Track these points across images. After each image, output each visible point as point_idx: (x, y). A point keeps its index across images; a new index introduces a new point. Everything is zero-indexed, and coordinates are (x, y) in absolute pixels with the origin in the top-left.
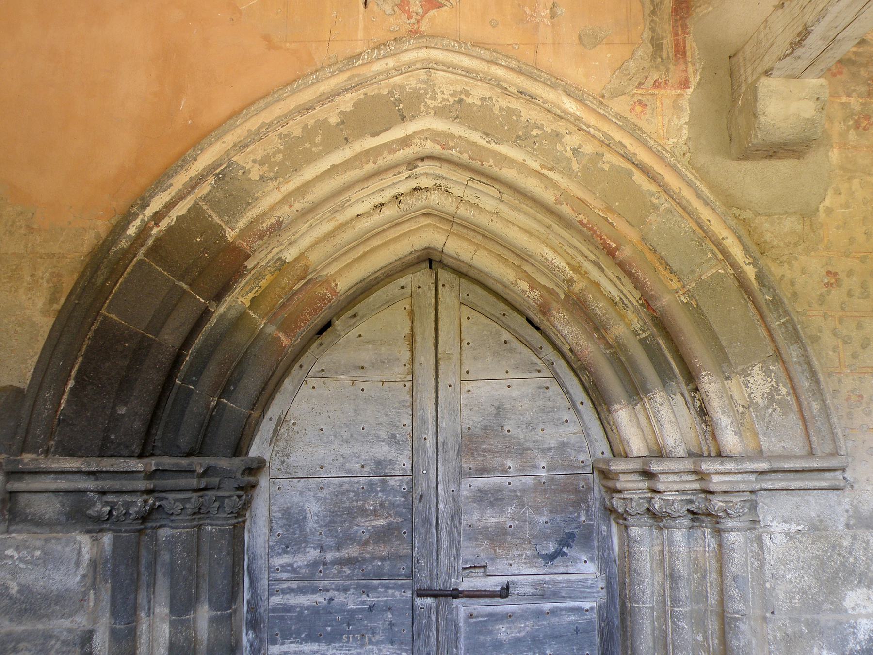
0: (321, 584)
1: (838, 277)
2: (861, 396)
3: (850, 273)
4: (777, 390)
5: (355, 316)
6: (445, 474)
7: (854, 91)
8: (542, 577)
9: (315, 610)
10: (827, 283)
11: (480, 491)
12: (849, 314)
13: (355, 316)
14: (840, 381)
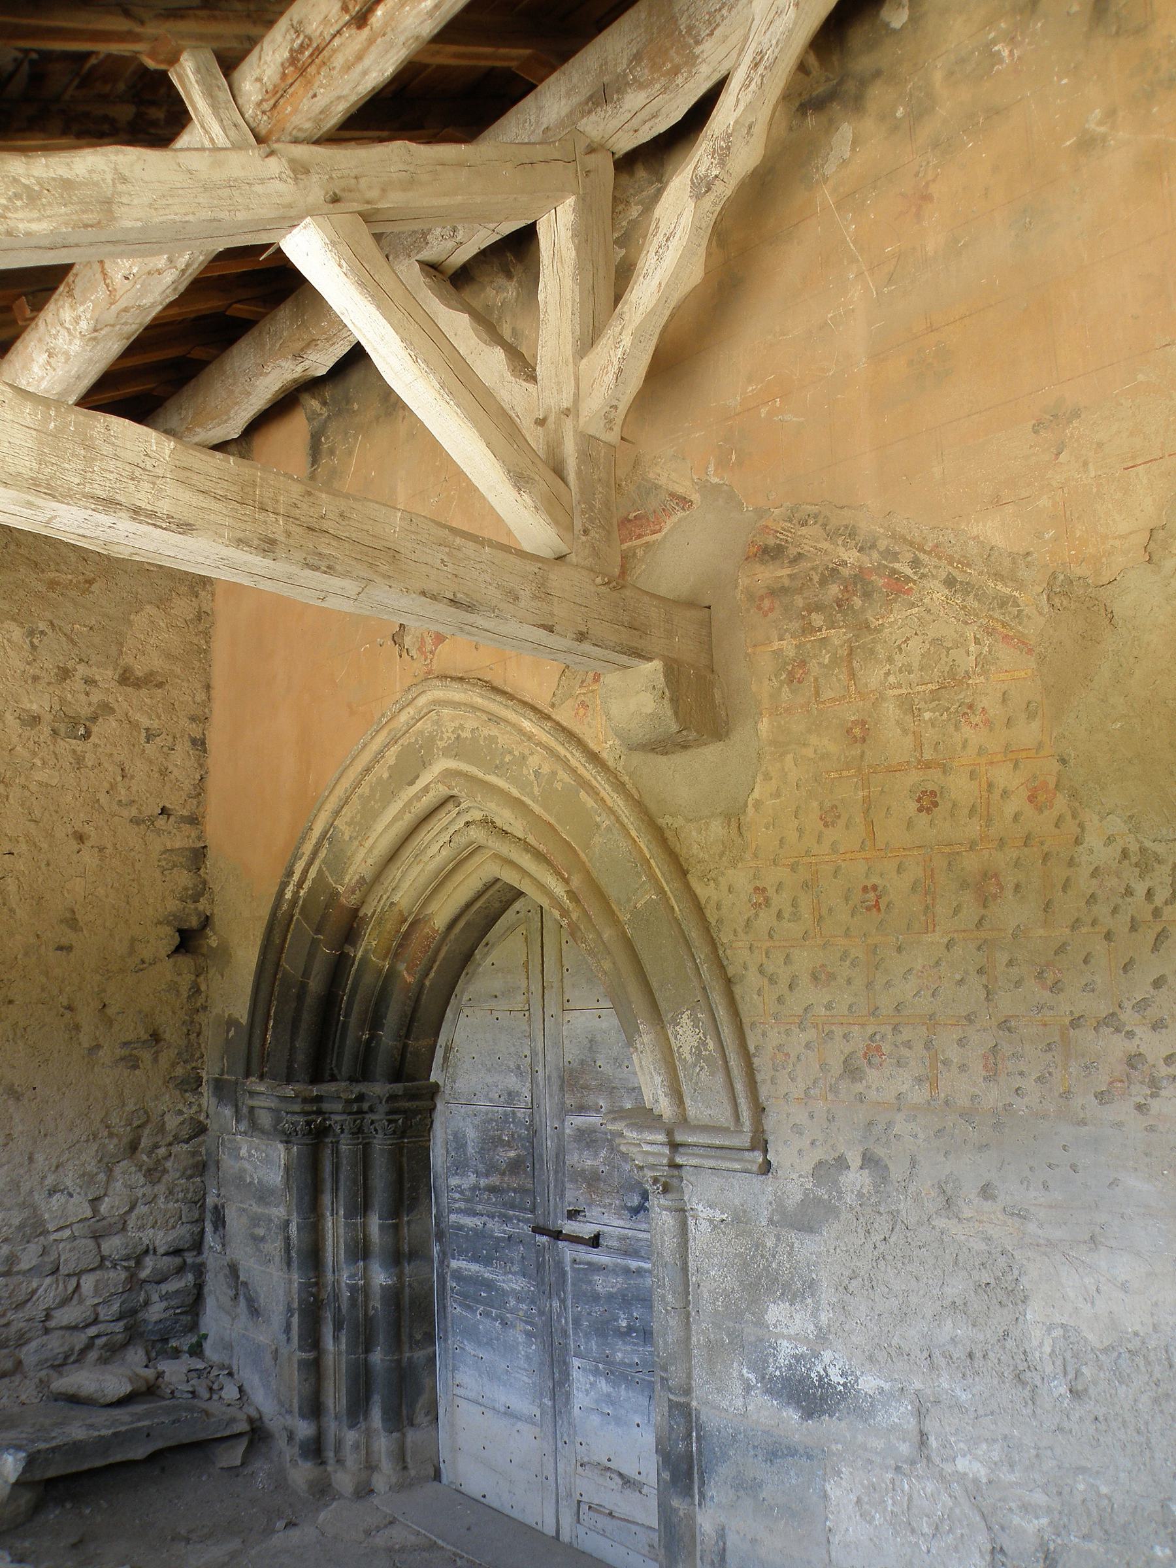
0: (479, 1208)
1: (767, 894)
2: (787, 1055)
3: (779, 887)
4: (705, 1044)
5: (487, 944)
6: (551, 1109)
7: (787, 630)
8: (626, 1231)
10: (755, 904)
12: (777, 944)
13: (487, 944)
14: (764, 1034)
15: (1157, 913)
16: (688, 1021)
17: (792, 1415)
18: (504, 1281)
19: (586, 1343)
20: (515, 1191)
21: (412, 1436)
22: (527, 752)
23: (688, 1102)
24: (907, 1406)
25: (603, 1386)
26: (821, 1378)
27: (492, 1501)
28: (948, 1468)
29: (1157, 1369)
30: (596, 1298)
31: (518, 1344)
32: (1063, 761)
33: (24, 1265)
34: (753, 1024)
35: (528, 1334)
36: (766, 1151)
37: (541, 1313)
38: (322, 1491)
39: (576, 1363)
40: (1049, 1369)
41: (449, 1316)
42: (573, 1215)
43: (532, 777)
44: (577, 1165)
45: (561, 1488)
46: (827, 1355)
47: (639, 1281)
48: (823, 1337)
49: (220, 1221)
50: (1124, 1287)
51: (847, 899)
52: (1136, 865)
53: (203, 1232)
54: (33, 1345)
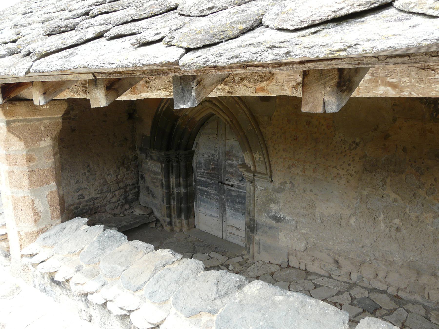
0: (205, 176)
4: (261, 158)
9: (204, 181)
11: (229, 164)
15: (345, 151)
17: (274, 222)
20: (214, 174)
21: (190, 220)
23: (257, 167)
24: (294, 222)
25: (233, 212)
26: (279, 217)
27: (207, 231)
28: (300, 231)
29: (335, 220)
30: (232, 196)
32: (334, 122)
33: (105, 191)
34: (271, 156)
35: (216, 201)
36: (272, 178)
37: (220, 198)
38: (172, 230)
39: (227, 207)
40: (318, 218)
42: (227, 180)
45: (223, 230)
46: (281, 213)
47: (241, 193)
48: (280, 210)
49: (143, 177)
50: (332, 208)
51: (291, 137)
52: (344, 142)
53: (138, 179)
54: (108, 206)
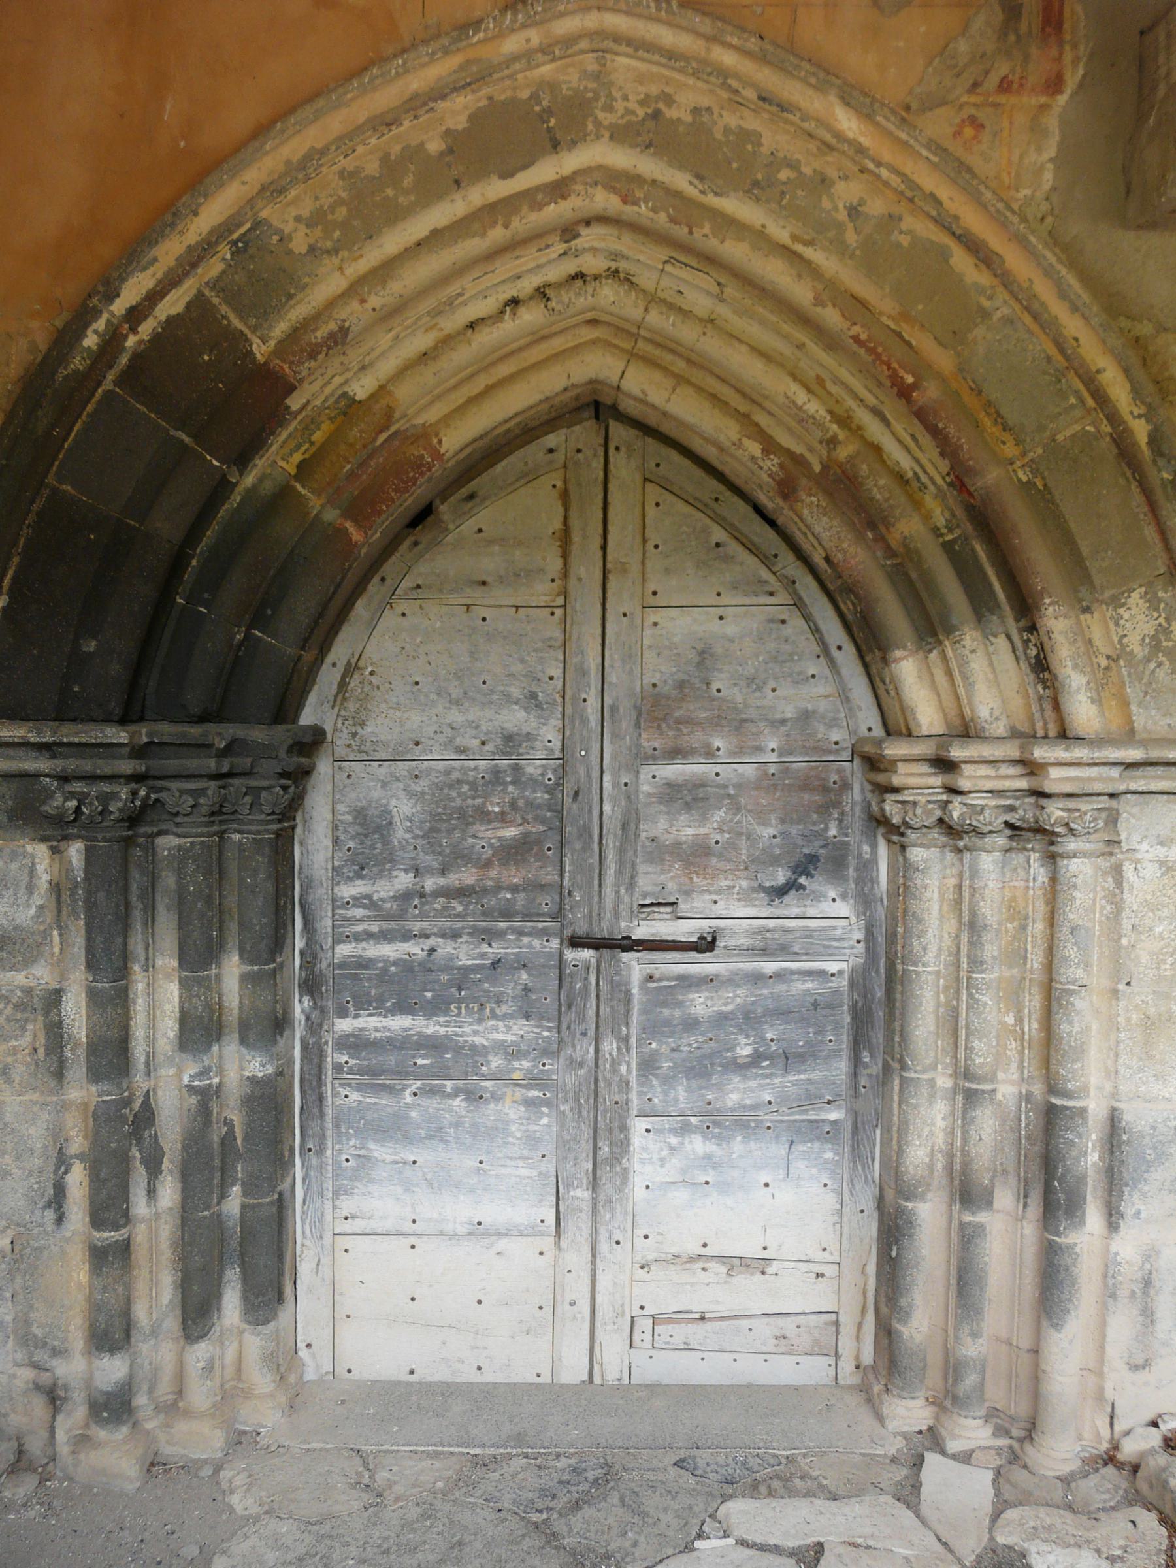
16: (1141, 602)
18: (476, 1033)
19: (665, 1093)
22: (832, 173)
30: (691, 1024)
31: (507, 1123)
41: (329, 1111)
43: (842, 215)
44: (662, 838)
